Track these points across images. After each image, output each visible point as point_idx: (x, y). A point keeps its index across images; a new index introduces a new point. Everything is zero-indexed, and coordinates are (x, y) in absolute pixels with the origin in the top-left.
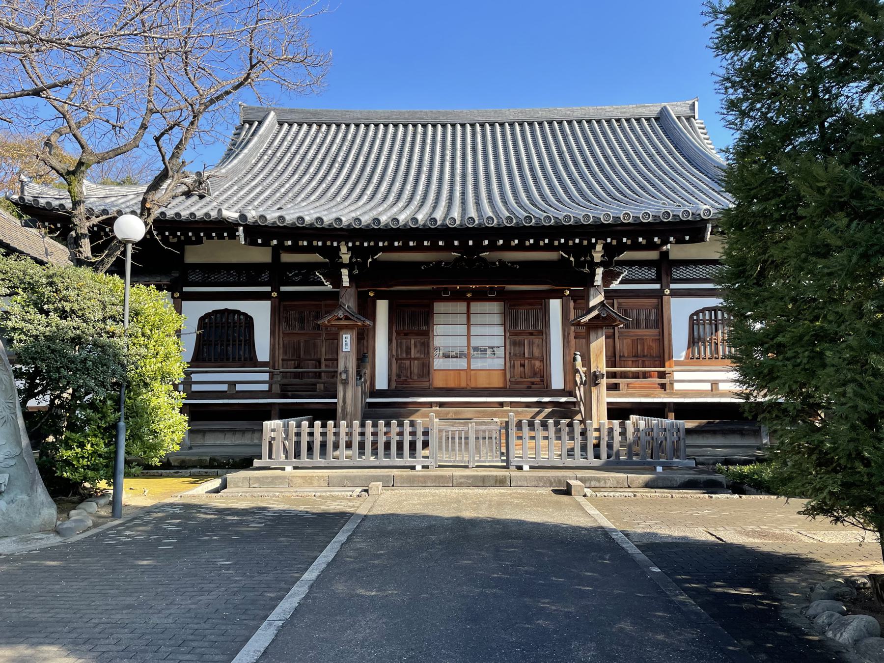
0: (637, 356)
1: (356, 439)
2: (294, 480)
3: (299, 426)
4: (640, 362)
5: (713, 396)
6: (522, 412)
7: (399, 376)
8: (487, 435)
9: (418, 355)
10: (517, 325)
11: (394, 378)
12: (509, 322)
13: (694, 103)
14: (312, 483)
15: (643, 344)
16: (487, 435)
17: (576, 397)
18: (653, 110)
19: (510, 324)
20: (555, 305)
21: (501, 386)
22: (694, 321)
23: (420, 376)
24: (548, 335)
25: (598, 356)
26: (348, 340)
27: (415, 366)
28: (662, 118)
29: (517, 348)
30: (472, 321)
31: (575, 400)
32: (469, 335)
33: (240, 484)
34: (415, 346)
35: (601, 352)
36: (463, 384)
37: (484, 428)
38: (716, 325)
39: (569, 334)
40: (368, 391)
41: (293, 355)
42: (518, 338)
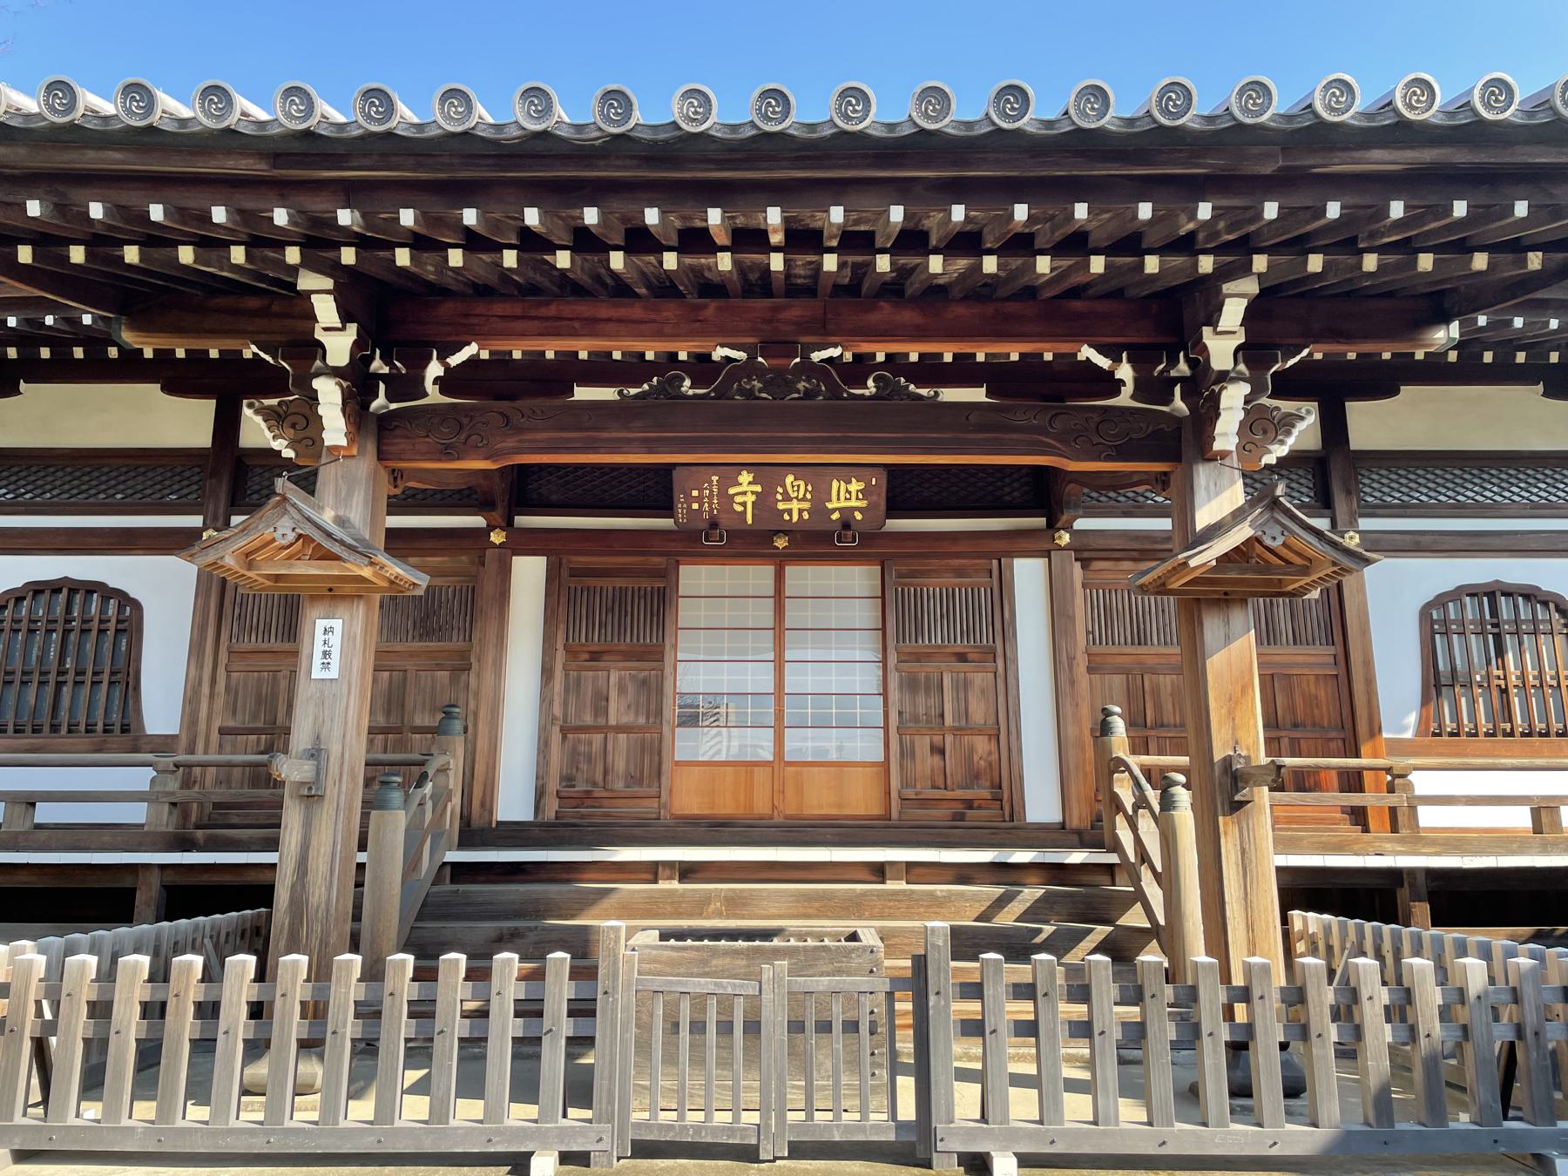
3: (107, 975)
4: (1285, 742)
5: (1545, 849)
7: (568, 780)
8: (838, 1016)
9: (627, 719)
10: (919, 631)
11: (553, 785)
12: (899, 622)
16: (838, 1016)
17: (1116, 847)
19: (901, 636)
20: (1028, 574)
21: (876, 810)
22: (1436, 620)
23: (634, 779)
24: (1010, 661)
25: (1234, 703)
26: (336, 640)
27: (621, 752)
29: (921, 699)
30: (790, 619)
31: (1113, 858)
32: (779, 664)
34: (622, 689)
35: (1246, 688)
36: (761, 806)
37: (823, 983)
38: (1498, 639)
39: (1071, 659)
40: (451, 823)
41: (255, 717)
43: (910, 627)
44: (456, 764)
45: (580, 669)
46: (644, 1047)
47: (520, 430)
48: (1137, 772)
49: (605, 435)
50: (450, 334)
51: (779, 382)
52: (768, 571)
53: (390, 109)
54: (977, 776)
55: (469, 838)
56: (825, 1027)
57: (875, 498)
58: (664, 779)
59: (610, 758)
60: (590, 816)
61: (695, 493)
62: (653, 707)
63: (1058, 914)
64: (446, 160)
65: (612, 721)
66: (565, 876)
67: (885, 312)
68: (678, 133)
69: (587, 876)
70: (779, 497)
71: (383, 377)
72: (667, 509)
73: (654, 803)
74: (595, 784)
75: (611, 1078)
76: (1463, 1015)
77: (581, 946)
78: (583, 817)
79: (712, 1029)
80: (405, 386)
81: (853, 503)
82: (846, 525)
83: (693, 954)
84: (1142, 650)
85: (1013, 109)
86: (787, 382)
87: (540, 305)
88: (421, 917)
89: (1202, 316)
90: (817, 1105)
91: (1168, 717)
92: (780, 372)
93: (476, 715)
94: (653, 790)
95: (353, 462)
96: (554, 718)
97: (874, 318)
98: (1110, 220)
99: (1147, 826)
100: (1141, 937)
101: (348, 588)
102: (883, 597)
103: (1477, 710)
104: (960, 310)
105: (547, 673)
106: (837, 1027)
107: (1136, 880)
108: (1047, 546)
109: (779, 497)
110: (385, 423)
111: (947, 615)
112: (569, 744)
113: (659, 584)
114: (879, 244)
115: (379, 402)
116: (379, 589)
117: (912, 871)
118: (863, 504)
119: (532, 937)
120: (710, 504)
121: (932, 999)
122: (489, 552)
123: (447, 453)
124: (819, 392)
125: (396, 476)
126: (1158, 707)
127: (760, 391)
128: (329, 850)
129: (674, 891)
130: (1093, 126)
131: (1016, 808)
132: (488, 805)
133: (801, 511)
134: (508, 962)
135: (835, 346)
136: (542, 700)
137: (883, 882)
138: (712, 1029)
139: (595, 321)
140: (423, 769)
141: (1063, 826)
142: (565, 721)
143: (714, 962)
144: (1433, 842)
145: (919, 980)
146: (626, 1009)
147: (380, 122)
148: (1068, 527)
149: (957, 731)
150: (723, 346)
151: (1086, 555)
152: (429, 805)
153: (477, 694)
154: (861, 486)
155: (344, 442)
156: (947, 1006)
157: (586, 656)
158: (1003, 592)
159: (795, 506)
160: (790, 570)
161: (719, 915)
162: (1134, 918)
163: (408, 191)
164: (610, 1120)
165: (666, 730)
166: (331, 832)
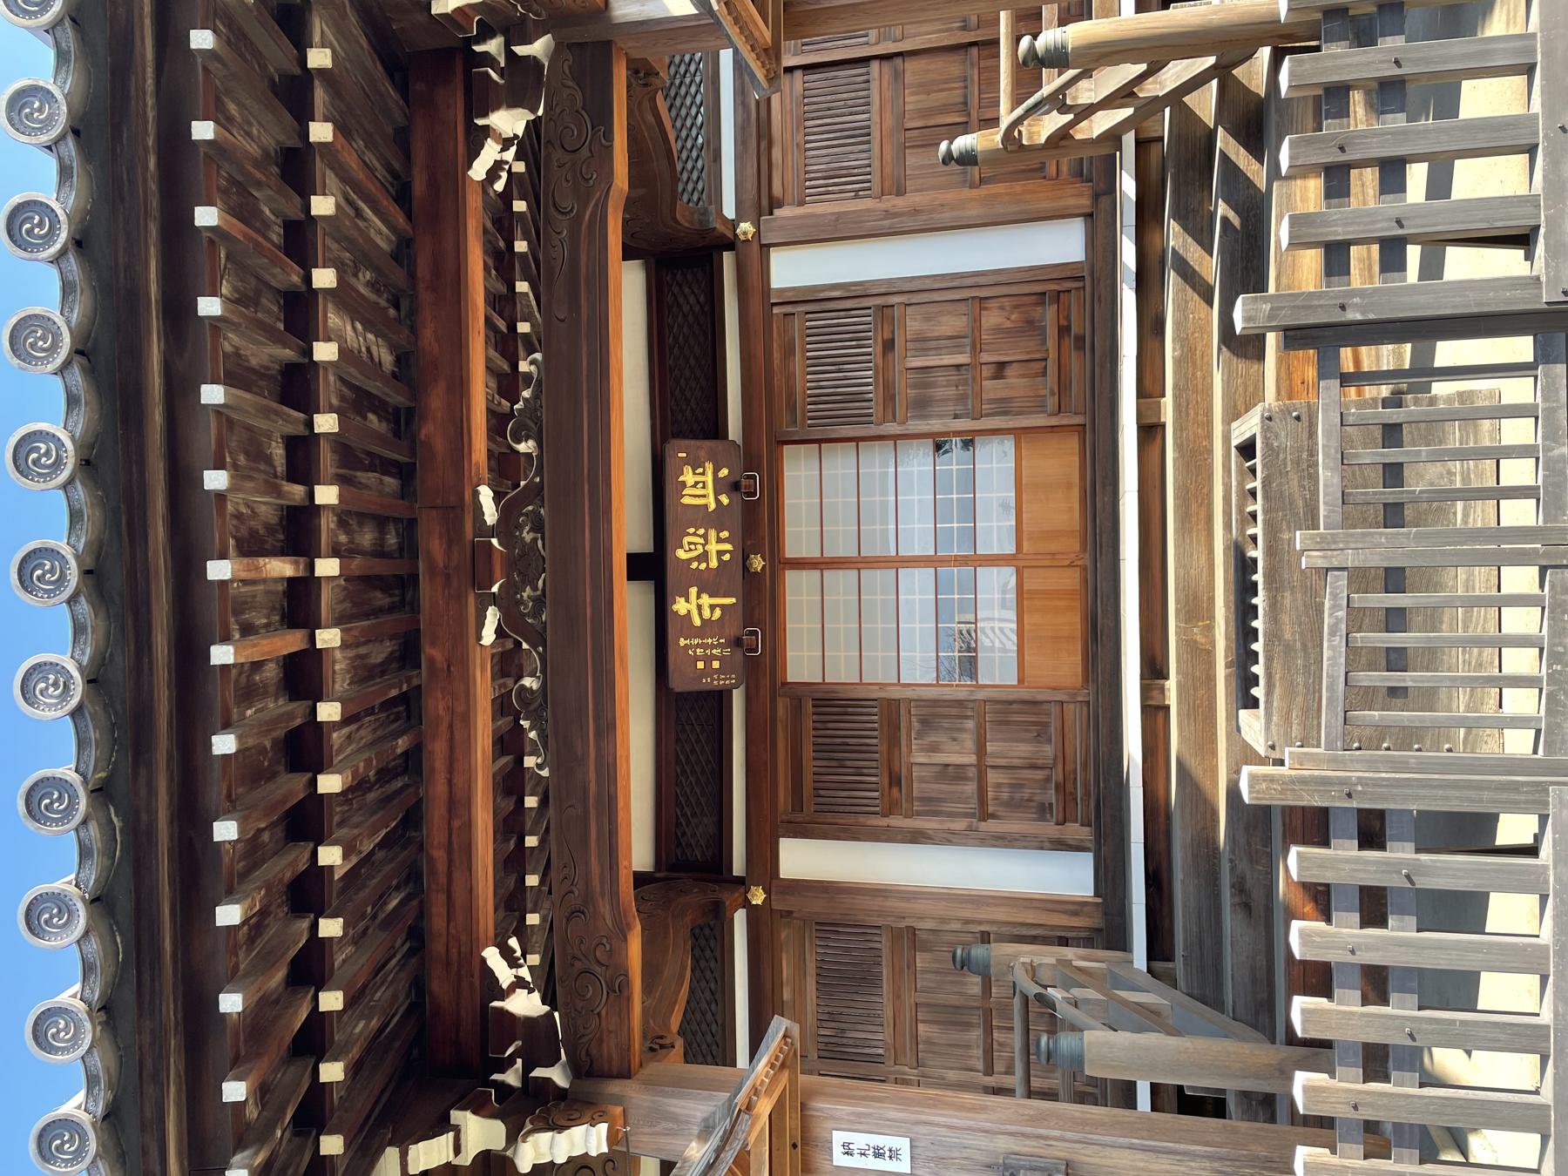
7: (1043, 811)
8: (1374, 455)
9: (969, 742)
11: (1050, 829)
12: (843, 423)
17: (1113, 137)
19: (865, 419)
20: (790, 270)
21: (1073, 443)
23: (1041, 734)
24: (891, 288)
26: (860, 1140)
27: (1008, 749)
29: (939, 393)
30: (846, 549)
31: (1129, 140)
34: (934, 748)
36: (1070, 580)
37: (1327, 477)
39: (888, 214)
42: (905, 391)
43: (854, 408)
44: (1026, 954)
45: (910, 798)
46: (1408, 737)
47: (588, 897)
48: (1020, 111)
49: (593, 787)
50: (472, 984)
51: (523, 564)
52: (791, 578)
53: (66, 1123)
54: (1030, 323)
55: (1117, 939)
56: (1393, 474)
57: (702, 453)
58: (1039, 698)
59: (1016, 762)
60: (1085, 784)
61: (700, 665)
62: (954, 711)
63: (1201, 203)
64: (147, 1039)
65: (972, 759)
66: (1162, 819)
67: (431, 430)
68: (88, 707)
69: (1161, 792)
70: (703, 566)
71: (527, 1069)
72: (720, 699)
73: (1068, 708)
74: (1048, 779)
75: (1480, 786)
77: (1265, 827)
78: (1087, 794)
79: (1397, 639)
80: (537, 1040)
81: (709, 478)
82: (734, 487)
83: (1277, 666)
84: (876, 133)
85: (41, 225)
86: (523, 556)
87: (433, 871)
88: (1217, 1004)
89: (420, 18)
90: (1492, 483)
91: (955, 96)
92: (511, 564)
93: (967, 922)
94: (1054, 709)
95: (631, 1111)
96: (970, 829)
97: (440, 445)
98: (239, 104)
99: (1086, 93)
100: (1230, 92)
101: (791, 1123)
102: (819, 441)
104: (428, 334)
105: (916, 837)
106: (1392, 455)
107: (1157, 103)
108: (756, 247)
109: (703, 566)
110: (579, 1070)
111: (838, 366)
112: (1001, 811)
113: (809, 706)
114: (300, 430)
115: (557, 1075)
116: (793, 1081)
117: (1148, 390)
118: (709, 467)
119: (1243, 866)
120: (713, 647)
121: (1353, 315)
122: (775, 906)
123: (619, 989)
124: (536, 513)
125: (657, 1046)
126: (944, 109)
127: (535, 588)
128: (1140, 1155)
129: (1180, 687)
130: (65, 108)
131: (1069, 274)
132: (1074, 907)
133: (719, 541)
134: (1303, 937)
135: (476, 494)
136: (949, 842)
137: (1163, 426)
138: (1397, 639)
139: (452, 803)
140: (1031, 997)
141: (1089, 216)
142: (972, 815)
143: (1288, 636)
145: (1317, 337)
146: (1372, 765)
147: (83, 1139)
148: (734, 224)
149: (976, 349)
150: (479, 638)
151: (765, 202)
152: (1077, 992)
153: (943, 920)
154: (688, 470)
155: (603, 1128)
156: (1360, 293)
157: (895, 790)
158: (811, 299)
159: (713, 547)
160: (790, 552)
161: (1209, 629)
162: (1205, 104)
163: (200, 1091)
164: (1543, 788)
165: (981, 695)
166: (1115, 1153)
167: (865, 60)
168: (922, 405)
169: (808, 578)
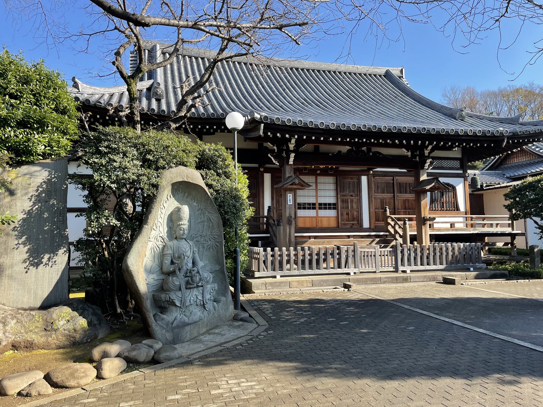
0: (405, 209)
1: (293, 258)
2: (292, 283)
5: (452, 230)
6: (364, 241)
12: (339, 188)
13: (402, 70)
14: (303, 285)
15: (408, 203)
17: (388, 231)
18: (382, 71)
19: (340, 192)
20: (364, 179)
28: (388, 75)
30: (319, 187)
31: (388, 233)
33: (260, 287)
52: (314, 177)
76: (460, 251)
103: (438, 205)
111: (349, 187)
144: (436, 230)
167: (394, 193)
168: (343, 201)
169: (314, 180)
